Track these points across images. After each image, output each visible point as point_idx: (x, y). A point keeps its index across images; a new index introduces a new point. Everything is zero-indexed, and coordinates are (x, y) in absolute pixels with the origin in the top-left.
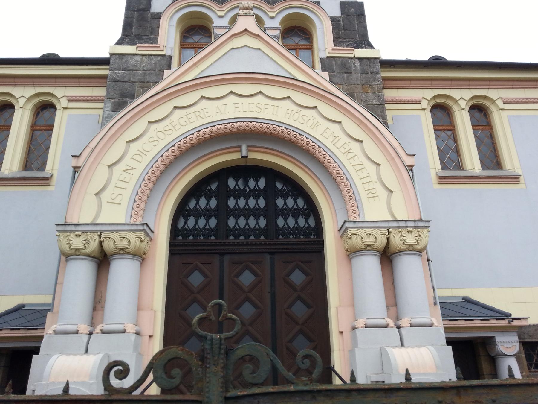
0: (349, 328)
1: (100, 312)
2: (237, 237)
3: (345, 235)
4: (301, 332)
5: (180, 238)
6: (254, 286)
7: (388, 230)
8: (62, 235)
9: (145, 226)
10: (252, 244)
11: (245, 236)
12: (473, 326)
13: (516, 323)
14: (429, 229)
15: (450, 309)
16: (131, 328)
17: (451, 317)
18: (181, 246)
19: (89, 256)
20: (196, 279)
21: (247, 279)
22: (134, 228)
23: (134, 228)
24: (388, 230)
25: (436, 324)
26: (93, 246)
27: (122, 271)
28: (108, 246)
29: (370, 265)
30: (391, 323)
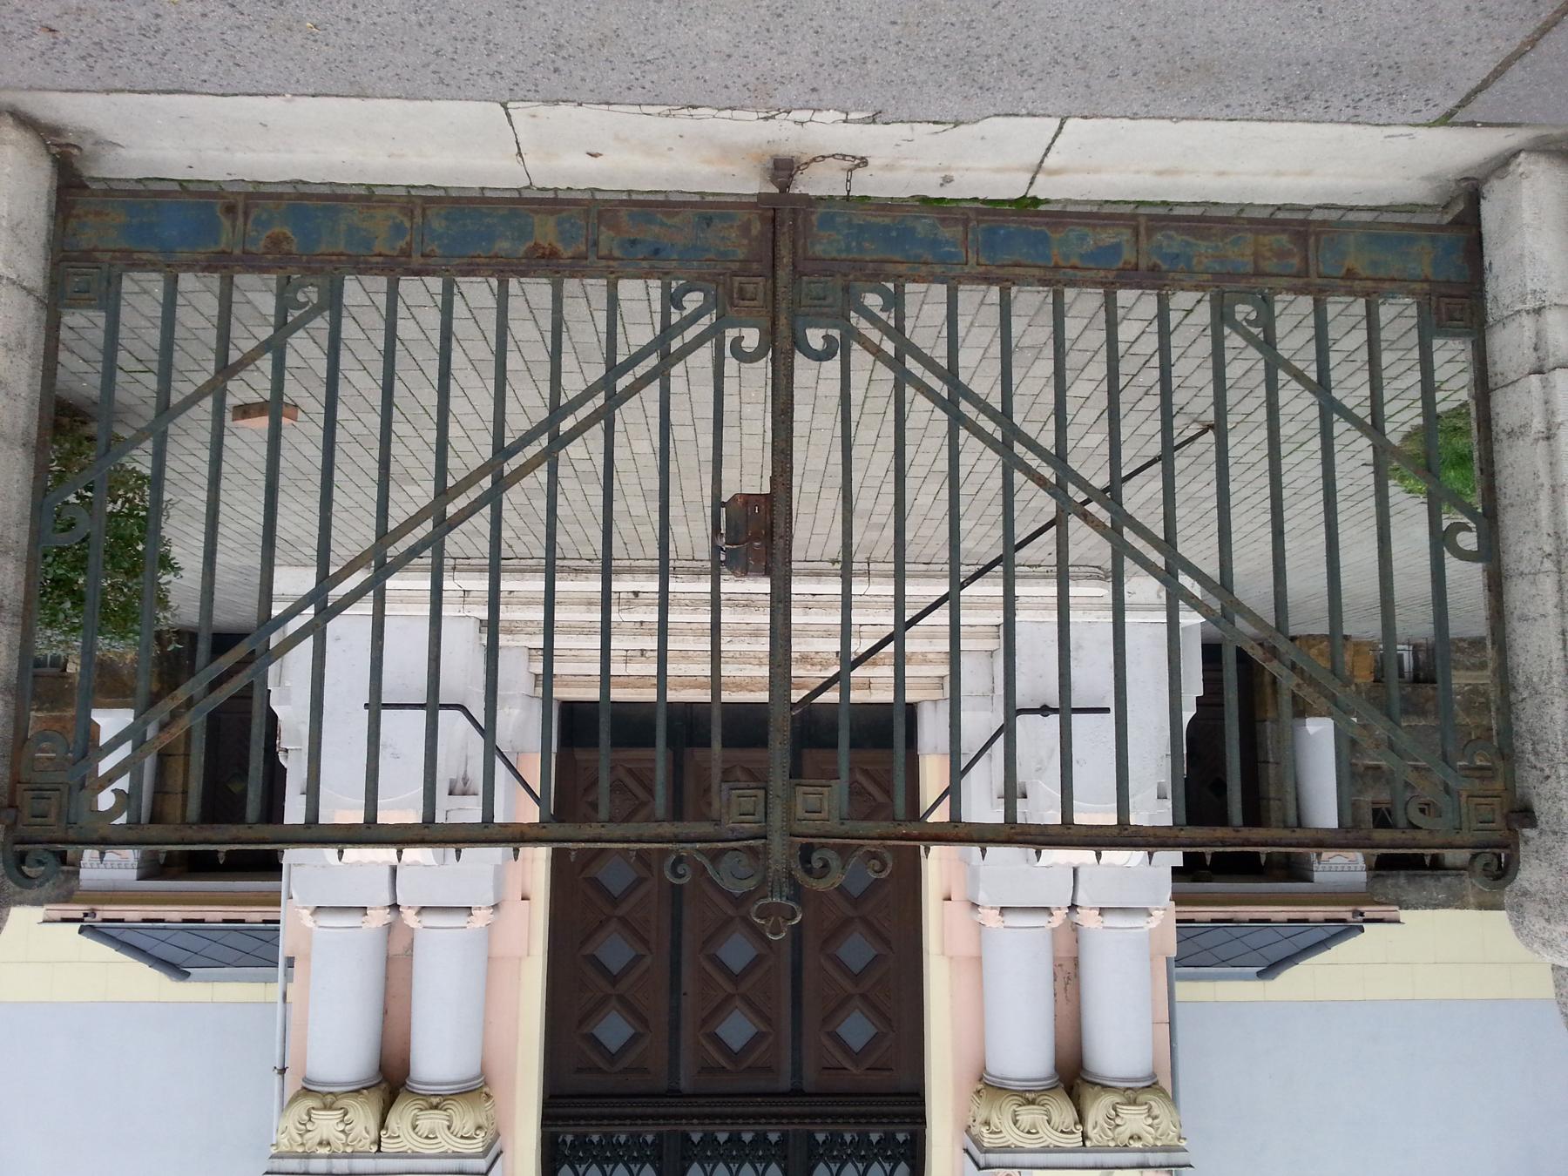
0: (505, 908)
1: (1063, 954)
2: (760, 1139)
3: (489, 1137)
4: (614, 901)
5: (901, 1137)
6: (719, 1010)
7: (379, 1150)
8: (1170, 1139)
9: (982, 1163)
10: (723, 1117)
11: (740, 1139)
12: (211, 905)
13: (77, 910)
14: (273, 1151)
15: (257, 950)
16: (991, 918)
17: (236, 930)
18: (896, 1115)
19: (1104, 1087)
20: (857, 1029)
21: (737, 1029)
22: (1007, 1158)
23: (1007, 1158)
24: (379, 1150)
25: (306, 913)
26: (1098, 1110)
27: (1026, 1053)
28: (1063, 1112)
29: (437, 1058)
30: (409, 917)
